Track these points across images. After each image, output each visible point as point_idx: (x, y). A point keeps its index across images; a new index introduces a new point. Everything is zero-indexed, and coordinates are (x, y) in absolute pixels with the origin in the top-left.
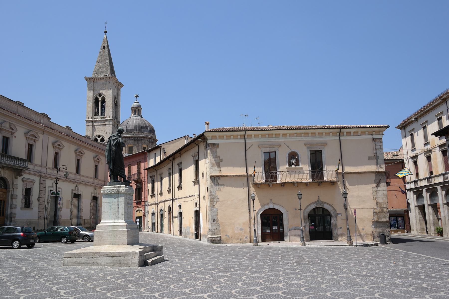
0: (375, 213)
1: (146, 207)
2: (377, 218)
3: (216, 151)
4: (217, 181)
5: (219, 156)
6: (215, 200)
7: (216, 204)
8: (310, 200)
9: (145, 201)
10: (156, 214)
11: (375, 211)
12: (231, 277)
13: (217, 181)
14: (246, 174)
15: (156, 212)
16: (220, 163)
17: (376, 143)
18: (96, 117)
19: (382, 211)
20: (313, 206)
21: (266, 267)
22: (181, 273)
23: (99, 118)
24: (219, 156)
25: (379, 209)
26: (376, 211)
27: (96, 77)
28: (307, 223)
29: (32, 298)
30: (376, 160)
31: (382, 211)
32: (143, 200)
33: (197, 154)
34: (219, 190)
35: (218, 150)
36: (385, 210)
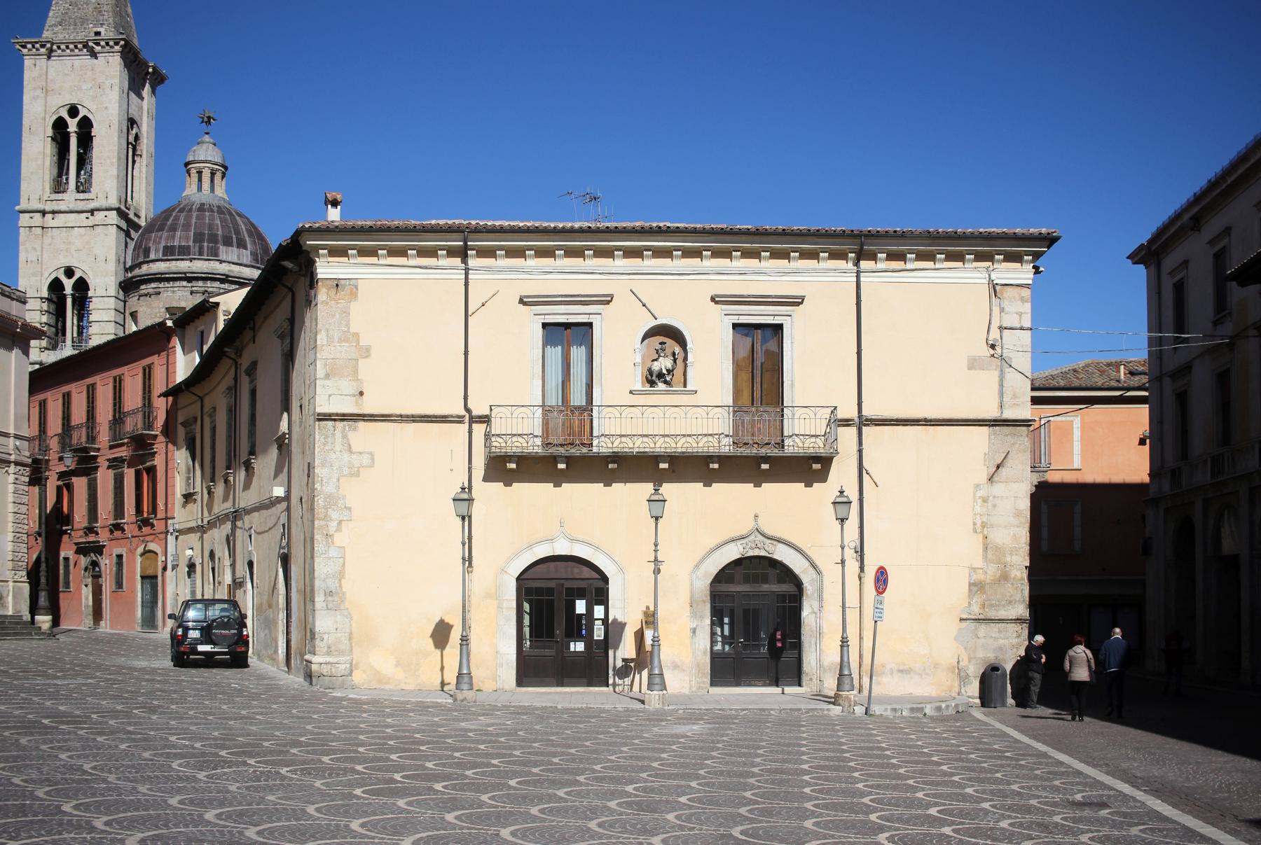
0: (977, 587)
1: (171, 539)
2: (983, 606)
3: (346, 313)
4: (344, 437)
5: (357, 335)
6: (334, 515)
7: (338, 529)
8: (715, 522)
9: (167, 519)
10: (198, 568)
11: (975, 578)
12: (544, 820)
13: (344, 437)
14: (463, 412)
15: (198, 561)
16: (361, 362)
17: (1006, 304)
18: (60, 196)
19: (1005, 577)
20: (733, 553)
21: (752, 781)
22: (358, 797)
23: (70, 198)
24: (357, 335)
25: (992, 571)
26: (980, 576)
27: (60, 37)
28: (702, 617)
29: (686, 843)
30: (997, 373)
31: (1005, 577)
32: (161, 515)
33: (286, 325)
34: (352, 475)
35: (355, 307)
36: (26, 488)
